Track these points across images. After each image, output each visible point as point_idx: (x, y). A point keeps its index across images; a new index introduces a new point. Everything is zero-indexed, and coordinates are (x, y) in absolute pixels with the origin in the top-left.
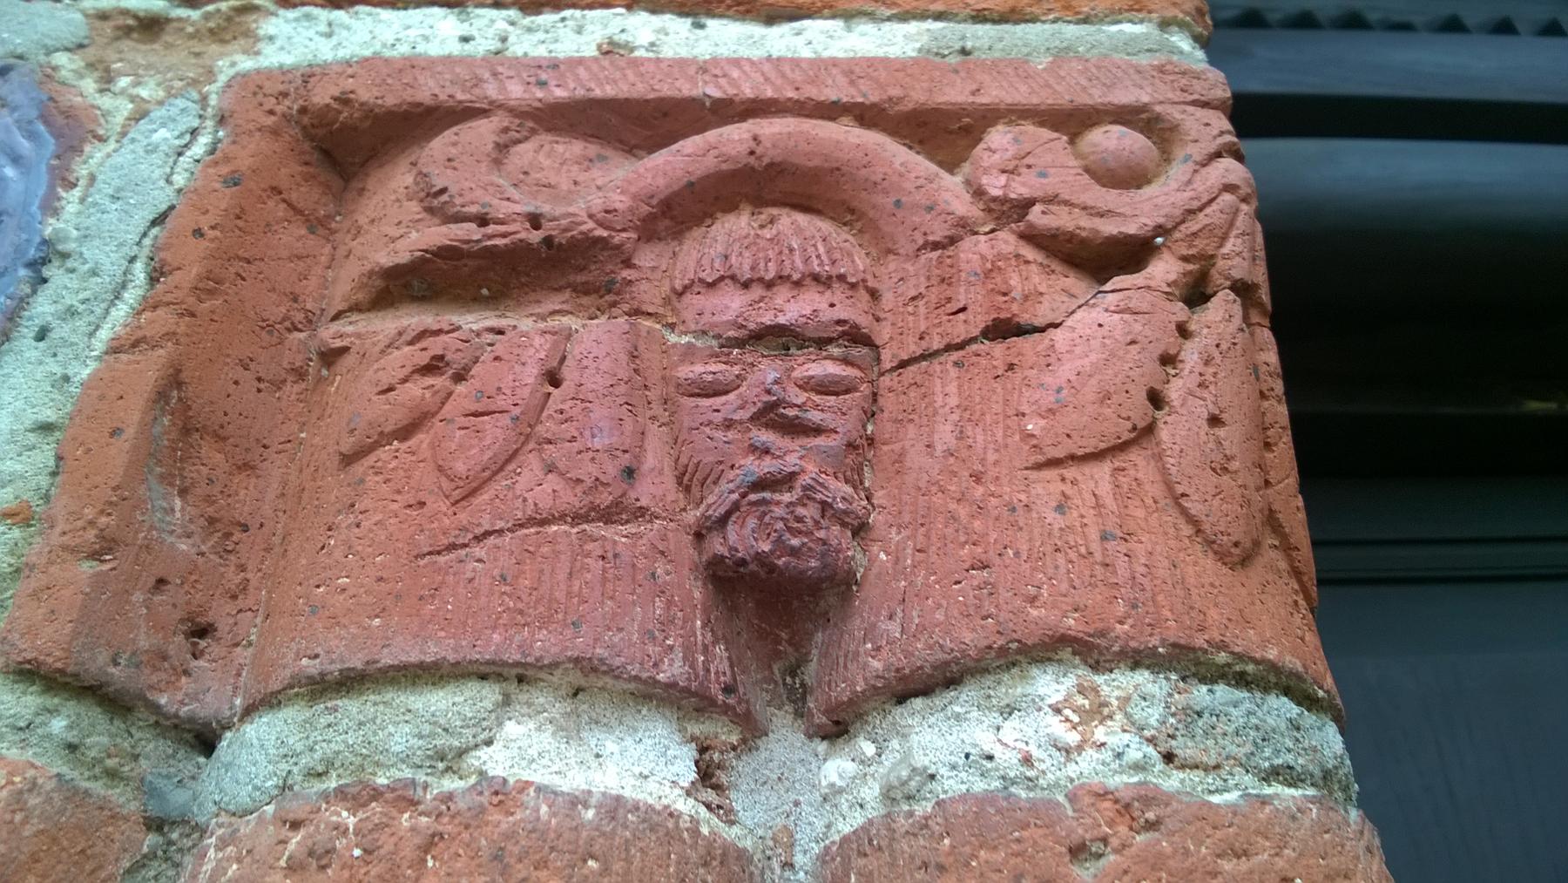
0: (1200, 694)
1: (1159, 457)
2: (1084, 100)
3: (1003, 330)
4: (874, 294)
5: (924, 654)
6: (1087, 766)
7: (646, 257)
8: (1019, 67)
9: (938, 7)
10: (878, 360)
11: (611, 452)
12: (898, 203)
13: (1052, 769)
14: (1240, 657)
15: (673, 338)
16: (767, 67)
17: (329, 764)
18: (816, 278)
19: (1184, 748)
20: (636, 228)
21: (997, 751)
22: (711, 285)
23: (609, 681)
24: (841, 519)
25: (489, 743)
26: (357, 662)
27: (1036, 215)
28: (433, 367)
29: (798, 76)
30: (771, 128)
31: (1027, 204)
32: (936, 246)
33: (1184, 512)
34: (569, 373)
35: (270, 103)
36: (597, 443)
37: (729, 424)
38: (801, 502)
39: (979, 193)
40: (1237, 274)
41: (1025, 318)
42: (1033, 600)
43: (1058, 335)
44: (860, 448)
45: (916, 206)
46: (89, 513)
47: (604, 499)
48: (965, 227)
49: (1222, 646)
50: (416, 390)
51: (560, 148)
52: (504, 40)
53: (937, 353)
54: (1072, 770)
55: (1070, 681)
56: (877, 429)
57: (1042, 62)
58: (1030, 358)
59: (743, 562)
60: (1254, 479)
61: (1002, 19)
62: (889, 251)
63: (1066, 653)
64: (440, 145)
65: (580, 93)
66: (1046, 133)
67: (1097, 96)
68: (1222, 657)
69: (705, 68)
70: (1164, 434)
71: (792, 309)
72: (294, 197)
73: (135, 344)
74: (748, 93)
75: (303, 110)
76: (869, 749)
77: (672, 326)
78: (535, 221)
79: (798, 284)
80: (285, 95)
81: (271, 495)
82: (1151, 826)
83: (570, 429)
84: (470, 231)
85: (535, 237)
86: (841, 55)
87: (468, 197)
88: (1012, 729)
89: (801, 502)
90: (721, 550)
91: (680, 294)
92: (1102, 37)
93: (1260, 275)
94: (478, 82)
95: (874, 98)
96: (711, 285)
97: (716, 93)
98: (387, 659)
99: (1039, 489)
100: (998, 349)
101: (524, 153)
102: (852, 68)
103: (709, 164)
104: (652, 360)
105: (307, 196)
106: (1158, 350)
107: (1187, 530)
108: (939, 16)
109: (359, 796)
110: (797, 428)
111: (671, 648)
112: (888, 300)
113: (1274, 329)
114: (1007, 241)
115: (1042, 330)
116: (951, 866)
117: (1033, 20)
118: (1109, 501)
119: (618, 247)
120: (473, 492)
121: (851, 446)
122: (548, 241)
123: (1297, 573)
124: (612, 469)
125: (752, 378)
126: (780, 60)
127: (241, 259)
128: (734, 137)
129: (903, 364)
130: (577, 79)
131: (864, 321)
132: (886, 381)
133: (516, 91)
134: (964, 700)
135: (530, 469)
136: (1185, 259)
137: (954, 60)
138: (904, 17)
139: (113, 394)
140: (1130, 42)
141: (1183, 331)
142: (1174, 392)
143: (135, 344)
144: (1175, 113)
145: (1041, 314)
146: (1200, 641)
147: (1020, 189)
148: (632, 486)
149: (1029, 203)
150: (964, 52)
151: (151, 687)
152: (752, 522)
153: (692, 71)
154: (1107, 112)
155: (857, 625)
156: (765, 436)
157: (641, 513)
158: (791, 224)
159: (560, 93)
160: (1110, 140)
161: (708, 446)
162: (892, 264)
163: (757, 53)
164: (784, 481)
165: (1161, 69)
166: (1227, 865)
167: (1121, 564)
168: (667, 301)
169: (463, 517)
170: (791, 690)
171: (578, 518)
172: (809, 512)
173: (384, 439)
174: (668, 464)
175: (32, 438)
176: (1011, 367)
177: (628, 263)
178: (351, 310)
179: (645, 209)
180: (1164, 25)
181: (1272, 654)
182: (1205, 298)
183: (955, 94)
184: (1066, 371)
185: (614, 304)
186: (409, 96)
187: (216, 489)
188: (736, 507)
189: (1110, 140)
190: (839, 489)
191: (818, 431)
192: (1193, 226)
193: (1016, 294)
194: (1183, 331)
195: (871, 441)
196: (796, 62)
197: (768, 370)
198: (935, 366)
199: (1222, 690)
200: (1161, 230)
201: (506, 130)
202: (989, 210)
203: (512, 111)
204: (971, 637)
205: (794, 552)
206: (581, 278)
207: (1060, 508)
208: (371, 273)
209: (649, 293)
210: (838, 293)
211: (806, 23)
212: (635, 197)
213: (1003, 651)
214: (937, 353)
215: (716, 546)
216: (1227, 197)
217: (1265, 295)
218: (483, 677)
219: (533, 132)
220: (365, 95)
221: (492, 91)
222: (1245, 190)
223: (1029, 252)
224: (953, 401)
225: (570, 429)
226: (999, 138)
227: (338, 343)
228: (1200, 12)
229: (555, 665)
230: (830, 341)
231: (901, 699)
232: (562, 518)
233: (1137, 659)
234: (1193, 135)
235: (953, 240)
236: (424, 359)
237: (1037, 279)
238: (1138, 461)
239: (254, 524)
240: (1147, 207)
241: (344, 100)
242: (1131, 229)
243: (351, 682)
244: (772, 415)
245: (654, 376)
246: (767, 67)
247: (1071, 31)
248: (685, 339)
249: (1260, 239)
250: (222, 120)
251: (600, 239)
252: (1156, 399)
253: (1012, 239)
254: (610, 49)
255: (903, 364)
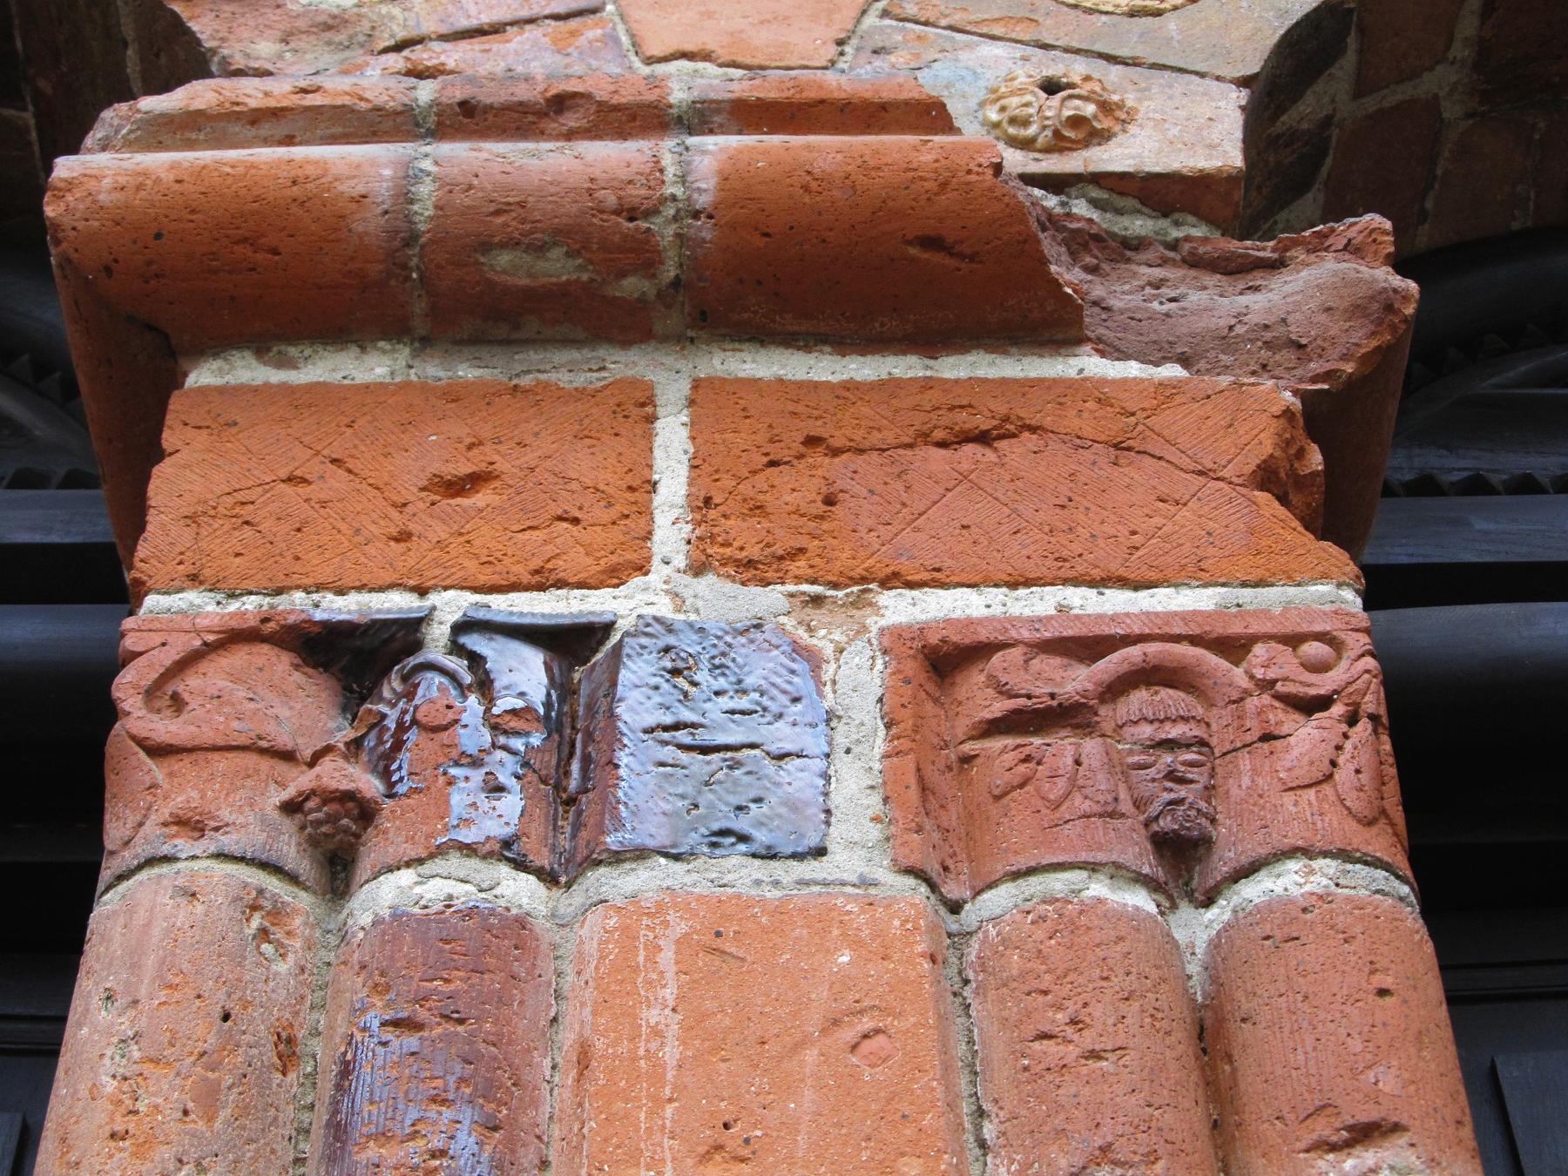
0: (1349, 867)
1: (1335, 786)
2: (1299, 630)
3: (1267, 737)
4: (1208, 725)
5: (1244, 860)
6: (1307, 888)
7: (1103, 711)
8: (1265, 614)
9: (1222, 580)
10: (1213, 753)
11: (1108, 791)
12: (1215, 683)
13: (1295, 892)
14: (1365, 854)
15: (1120, 747)
16: (1143, 617)
17: (1032, 896)
18: (1182, 718)
19: (1341, 881)
21: (1275, 888)
22: (1136, 723)
23: (1124, 872)
24: (1206, 815)
26: (1033, 864)
27: (1279, 686)
28: (1027, 759)
29: (1159, 622)
30: (1153, 648)
31: (1275, 682)
32: (1234, 702)
33: (1344, 805)
34: (1084, 759)
35: (909, 644)
36: (1102, 787)
37: (1154, 780)
38: (1189, 809)
39: (1252, 677)
40: (1370, 711)
41: (1277, 733)
42: (1285, 836)
43: (1291, 739)
44: (1209, 789)
45: (1223, 684)
46: (911, 817)
47: (1110, 809)
48: (1248, 692)
49: (1358, 850)
50: (1022, 768)
51: (1052, 661)
52: (1004, 605)
53: (1239, 749)
54: (1302, 891)
55: (1301, 863)
56: (1219, 780)
57: (1277, 610)
58: (1280, 749)
59: (1167, 833)
60: (1375, 794)
61: (1256, 585)
62: (1212, 705)
63: (1299, 855)
64: (997, 658)
65: (1057, 634)
66: (1281, 647)
67: (1305, 628)
68: (1358, 854)
69: (1114, 618)
70: (1337, 777)
71: (1175, 731)
73: (897, 754)
74: (1137, 631)
75: (924, 647)
76: (1225, 903)
77: (1119, 742)
78: (1052, 696)
79: (1174, 721)
80: (913, 639)
81: (954, 818)
82: (1330, 902)
83: (1090, 782)
84: (1022, 701)
85: (1055, 703)
86: (1178, 609)
87: (1019, 686)
88: (1280, 882)
89: (1189, 809)
90: (1157, 829)
91: (1121, 727)
92: (1307, 594)
93: (1382, 711)
94: (1007, 630)
95: (1198, 631)
96: (1136, 723)
97: (1122, 632)
98: (1044, 862)
99: (1285, 799)
100: (1266, 746)
101: (1036, 664)
102: (1186, 617)
103: (1125, 667)
104: (1115, 756)
105: (930, 687)
106: (1334, 743)
107: (1346, 812)
108: (1223, 585)
109: (1053, 901)
110: (1182, 781)
112: (1214, 727)
113: (1391, 736)
114: (1266, 699)
115: (1284, 737)
116: (1281, 797)
117: (1272, 585)
118: (1314, 802)
119: (1091, 707)
120: (1059, 806)
121: (1206, 788)
122: (1060, 705)
123: (1396, 834)
124: (1110, 799)
125: (1161, 761)
126: (1147, 614)
128: (1134, 652)
129: (1225, 754)
130: (1053, 627)
131: (1205, 736)
132: (1217, 761)
133: (1026, 634)
134: (1262, 875)
135: (1077, 799)
136: (1347, 705)
137: (1234, 610)
138: (1206, 585)
139: (899, 773)
140: (1321, 599)
141: (1346, 736)
142: (1341, 760)
143: (897, 754)
144: (1342, 635)
145: (1285, 730)
146: (1349, 848)
147: (1271, 675)
149: (1276, 681)
150: (1238, 605)
152: (1169, 818)
153: (1107, 620)
155: (1215, 858)
156: (1169, 784)
157: (1122, 815)
158: (1165, 693)
159: (1048, 635)
160: (1314, 649)
161: (1147, 789)
162: (1215, 711)
163: (1134, 610)
164: (1180, 801)
165: (1336, 613)
166: (1356, 912)
167: (1319, 825)
168: (1115, 731)
169: (1058, 815)
170: (1186, 892)
171: (1101, 816)
172: (1193, 813)
173: (1014, 788)
174: (1128, 797)
175: (868, 791)
176: (1272, 753)
177: (1096, 714)
178: (969, 739)
179: (1100, 689)
180: (1339, 585)
181: (1378, 854)
182: (1357, 722)
183: (1236, 629)
184: (1295, 753)
185: (1091, 733)
186: (977, 638)
188: (1161, 812)
189: (1314, 649)
190: (1203, 805)
191: (1192, 781)
192: (1350, 689)
193: (1272, 722)
194: (1346, 736)
195: (1214, 787)
196: (1157, 614)
197: (1168, 758)
198: (1239, 754)
199: (1358, 866)
200: (1335, 692)
201: (1025, 654)
202: (1257, 685)
203: (1026, 644)
204: (1263, 851)
205: (1188, 829)
206: (1074, 721)
207: (1295, 805)
208: (980, 722)
209: (1108, 727)
210: (1193, 724)
211: (1155, 590)
212: (1095, 684)
213: (1275, 855)
214: (1239, 749)
215: (1155, 827)
216: (1367, 676)
217: (1385, 720)
218: (1080, 868)
219: (1037, 654)
220: (955, 638)
221: (1014, 634)
222: (1375, 672)
223: (1277, 704)
224: (1248, 767)
225: (1090, 782)
226: (1259, 650)
227: (973, 753)
228: (1358, 577)
229: (1106, 864)
230: (1192, 745)
231: (1236, 882)
232: (1095, 815)
233: (1325, 854)
234: (1351, 646)
235: (1242, 699)
236: (1023, 756)
237: (1281, 716)
238: (1327, 788)
239: (951, 829)
240: (1329, 682)
241: (943, 641)
242: (1322, 692)
243: (1031, 871)
244: (1172, 776)
245: (1116, 762)
246: (1143, 617)
247: (1292, 591)
248: (1127, 746)
249: (1382, 694)
250: (885, 653)
251: (1084, 704)
252: (1334, 764)
253: (1269, 698)
254: (1062, 609)
255: (1225, 754)
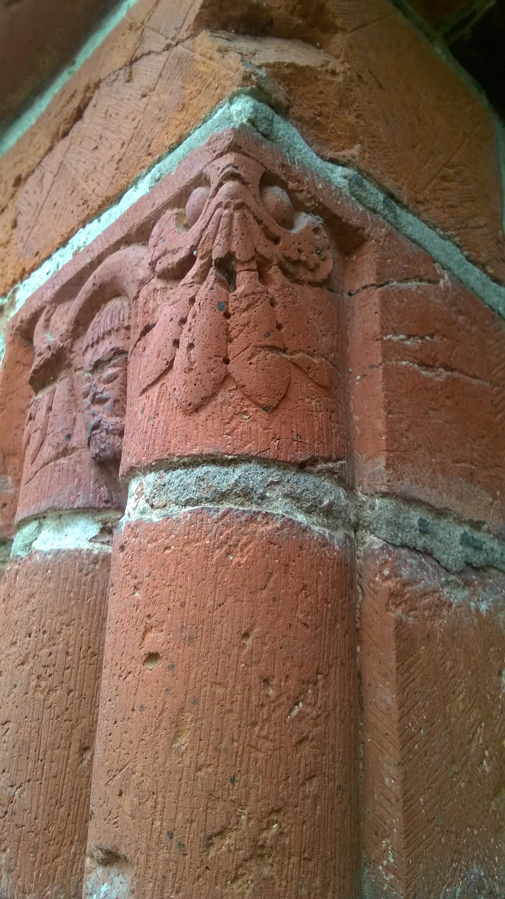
20: (70, 337)
25: (36, 539)
68: (175, 459)
72: (24, 361)
111: (79, 495)
124: (62, 437)
127: (10, 393)
148: (69, 441)
151: (9, 535)
154: (191, 185)
157: (74, 449)
187: (17, 471)
219: (56, 307)
